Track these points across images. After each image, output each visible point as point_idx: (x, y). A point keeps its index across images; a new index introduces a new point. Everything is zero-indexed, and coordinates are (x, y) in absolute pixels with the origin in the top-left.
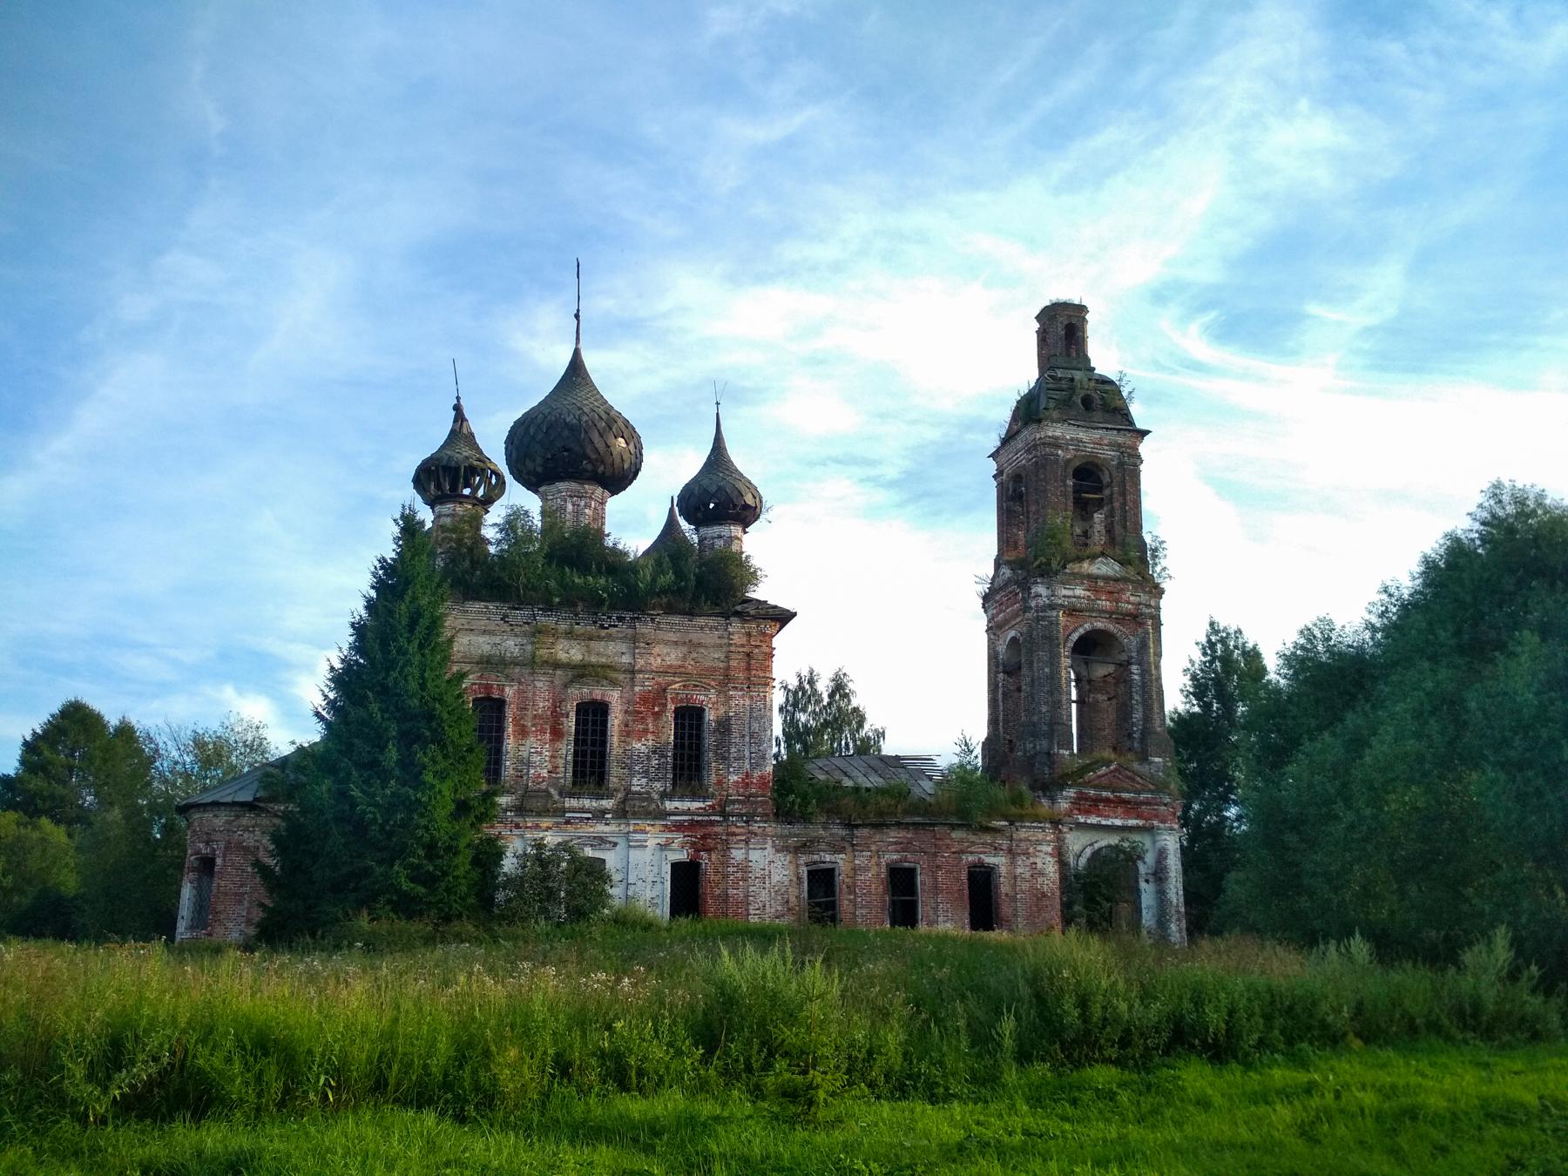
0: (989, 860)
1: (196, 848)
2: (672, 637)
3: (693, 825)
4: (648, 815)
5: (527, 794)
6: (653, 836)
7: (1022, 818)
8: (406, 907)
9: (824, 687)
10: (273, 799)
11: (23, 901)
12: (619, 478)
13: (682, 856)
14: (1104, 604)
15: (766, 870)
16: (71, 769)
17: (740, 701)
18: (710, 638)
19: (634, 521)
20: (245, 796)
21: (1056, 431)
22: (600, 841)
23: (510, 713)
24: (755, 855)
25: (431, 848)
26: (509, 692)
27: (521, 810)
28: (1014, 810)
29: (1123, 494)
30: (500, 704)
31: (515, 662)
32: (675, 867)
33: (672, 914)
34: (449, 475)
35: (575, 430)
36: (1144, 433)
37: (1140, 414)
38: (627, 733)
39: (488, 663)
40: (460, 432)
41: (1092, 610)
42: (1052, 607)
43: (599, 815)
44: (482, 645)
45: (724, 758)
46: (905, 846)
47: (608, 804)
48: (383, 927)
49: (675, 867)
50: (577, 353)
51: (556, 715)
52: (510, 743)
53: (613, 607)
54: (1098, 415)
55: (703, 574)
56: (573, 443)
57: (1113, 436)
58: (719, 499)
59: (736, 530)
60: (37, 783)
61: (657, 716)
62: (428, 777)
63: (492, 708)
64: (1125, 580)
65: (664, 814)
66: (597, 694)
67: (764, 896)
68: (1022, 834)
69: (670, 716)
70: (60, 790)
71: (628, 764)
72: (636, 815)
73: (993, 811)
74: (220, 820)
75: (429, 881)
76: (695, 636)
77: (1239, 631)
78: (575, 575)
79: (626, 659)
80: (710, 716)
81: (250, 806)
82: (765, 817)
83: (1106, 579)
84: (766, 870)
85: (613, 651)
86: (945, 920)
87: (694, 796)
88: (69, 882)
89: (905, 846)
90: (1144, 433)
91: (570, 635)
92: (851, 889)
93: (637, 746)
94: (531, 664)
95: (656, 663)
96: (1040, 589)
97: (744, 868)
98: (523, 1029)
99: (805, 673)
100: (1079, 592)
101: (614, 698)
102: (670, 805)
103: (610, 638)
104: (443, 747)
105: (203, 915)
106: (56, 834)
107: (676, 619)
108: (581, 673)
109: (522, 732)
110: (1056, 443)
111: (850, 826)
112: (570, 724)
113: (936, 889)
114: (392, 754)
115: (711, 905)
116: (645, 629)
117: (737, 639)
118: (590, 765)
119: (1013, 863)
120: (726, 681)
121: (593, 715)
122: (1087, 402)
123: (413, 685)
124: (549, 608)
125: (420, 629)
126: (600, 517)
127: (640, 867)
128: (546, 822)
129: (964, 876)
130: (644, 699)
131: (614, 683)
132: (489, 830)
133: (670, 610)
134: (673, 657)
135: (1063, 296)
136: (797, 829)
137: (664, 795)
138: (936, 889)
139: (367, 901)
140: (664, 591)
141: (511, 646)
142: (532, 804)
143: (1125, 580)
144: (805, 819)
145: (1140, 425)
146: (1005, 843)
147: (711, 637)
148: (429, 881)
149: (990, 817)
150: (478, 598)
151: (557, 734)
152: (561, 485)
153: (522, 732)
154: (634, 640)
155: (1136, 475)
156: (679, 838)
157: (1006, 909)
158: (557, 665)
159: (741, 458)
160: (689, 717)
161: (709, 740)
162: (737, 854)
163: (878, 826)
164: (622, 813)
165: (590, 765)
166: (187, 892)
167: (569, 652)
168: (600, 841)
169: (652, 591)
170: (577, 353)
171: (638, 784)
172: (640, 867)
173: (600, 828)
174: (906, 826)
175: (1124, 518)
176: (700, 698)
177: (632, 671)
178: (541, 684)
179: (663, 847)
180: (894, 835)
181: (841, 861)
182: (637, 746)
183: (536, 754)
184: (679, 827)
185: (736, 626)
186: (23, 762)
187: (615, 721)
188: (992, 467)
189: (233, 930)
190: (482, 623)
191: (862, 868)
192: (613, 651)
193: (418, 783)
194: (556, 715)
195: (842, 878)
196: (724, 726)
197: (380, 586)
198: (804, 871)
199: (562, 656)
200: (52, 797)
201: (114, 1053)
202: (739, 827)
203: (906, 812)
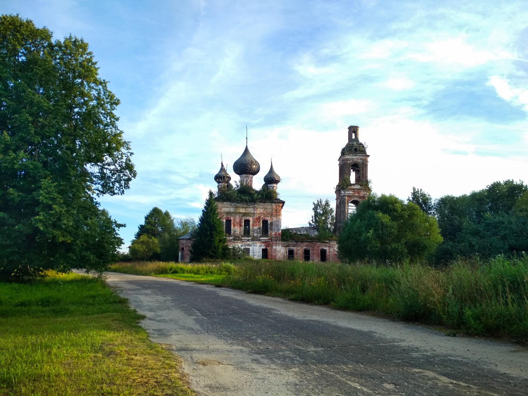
0: (325, 248)
1: (181, 246)
2: (261, 207)
3: (266, 242)
4: (257, 240)
5: (235, 237)
6: (258, 244)
7: (331, 240)
8: (211, 257)
9: (323, 203)
10: (192, 238)
11: (151, 254)
12: (255, 173)
13: (264, 248)
14: (356, 195)
15: (280, 250)
16: (156, 223)
17: (274, 219)
18: (269, 207)
19: (257, 183)
20: (188, 237)
21: (347, 157)
22: (249, 245)
23: (232, 222)
24: (277, 247)
25: (215, 248)
26: (232, 218)
27: (234, 239)
28: (330, 238)
29: (363, 170)
30: (230, 220)
31: (233, 213)
32: (263, 250)
33: (262, 258)
34: (221, 177)
35: (245, 165)
36: (369, 156)
37: (368, 152)
38: (253, 225)
39: (228, 213)
40: (223, 169)
41: (354, 196)
42: (344, 196)
43: (248, 240)
44: (227, 210)
45: (272, 230)
46: (307, 246)
47: (250, 238)
48: (207, 260)
49: (263, 250)
50: (247, 146)
51: (240, 222)
52: (232, 228)
53: (250, 202)
54: (358, 152)
55: (268, 196)
56: (245, 166)
57: (361, 157)
58: (271, 179)
59: (275, 185)
60: (149, 227)
61: (259, 222)
62: (214, 236)
63: (229, 222)
64: (361, 189)
65: (260, 240)
66: (248, 218)
67: (279, 255)
68: (332, 243)
69: (261, 222)
70: (154, 228)
71: (253, 231)
72: (255, 240)
73: (326, 239)
74: (184, 242)
75: (215, 253)
76: (266, 207)
77: (421, 190)
78: (245, 194)
79: (253, 211)
80: (269, 222)
81: (189, 239)
82: (279, 240)
83: (357, 189)
84: (280, 250)
85: (251, 210)
86: (315, 259)
87: (266, 237)
88: (159, 250)
89: (307, 246)
90: (369, 156)
91: (242, 207)
92: (297, 254)
93: (255, 228)
94: (235, 213)
95: (258, 212)
96: (342, 192)
97: (275, 250)
98: (203, 269)
99: (319, 200)
100: (351, 192)
101: (251, 219)
102: (261, 238)
103: (250, 208)
104: (216, 231)
105: (183, 258)
106: (156, 241)
107: (262, 204)
108: (244, 214)
109: (234, 226)
110: (347, 160)
111: (297, 242)
112: (243, 224)
113: (314, 254)
114: (209, 233)
115: (269, 257)
116: (256, 206)
117: (274, 207)
118: (247, 232)
119: (330, 249)
120: (272, 215)
121: (247, 222)
122: (356, 150)
123: (212, 221)
124: (238, 203)
125: (212, 212)
126: (251, 181)
127: (256, 250)
128: (239, 242)
129: (319, 251)
130: (256, 219)
131: (251, 216)
132: (226, 244)
133: (261, 202)
134: (262, 211)
135: (353, 124)
136: (286, 242)
137: (260, 237)
138: (314, 254)
139: (205, 256)
140: (259, 199)
141: (232, 210)
142: (237, 238)
143: (361, 189)
144: (287, 241)
145: (368, 154)
146: (328, 245)
147: (270, 207)
148: (215, 253)
149: (325, 240)
150: (226, 201)
151: (241, 226)
152: (243, 175)
153: (234, 226)
154: (254, 208)
155: (366, 166)
156: (263, 244)
157: (328, 257)
158: (240, 213)
159: (276, 170)
160: (265, 222)
161: (269, 226)
162: (274, 247)
163: (302, 242)
164: (252, 240)
165: (247, 232)
166: (180, 253)
167: (242, 211)
168: (249, 245)
169: (257, 199)
170: (247, 146)
171: (255, 235)
172: (256, 250)
173: (249, 243)
174: (308, 242)
175: (363, 175)
176: (267, 218)
177: (254, 214)
178: (237, 217)
179: (260, 246)
180: (305, 244)
181: (295, 248)
182: (255, 228)
183: (237, 230)
184: (263, 242)
185: (274, 205)
186: (145, 222)
187: (251, 223)
188: (338, 163)
189: (188, 260)
190: (227, 206)
191: (299, 250)
192: (251, 210)
193: (213, 237)
194: (240, 222)
195: (295, 252)
196: (271, 224)
197: (206, 203)
198: (287, 250)
199: (241, 211)
200: (152, 230)
201: (171, 269)
202: (275, 242)
203: (307, 239)
